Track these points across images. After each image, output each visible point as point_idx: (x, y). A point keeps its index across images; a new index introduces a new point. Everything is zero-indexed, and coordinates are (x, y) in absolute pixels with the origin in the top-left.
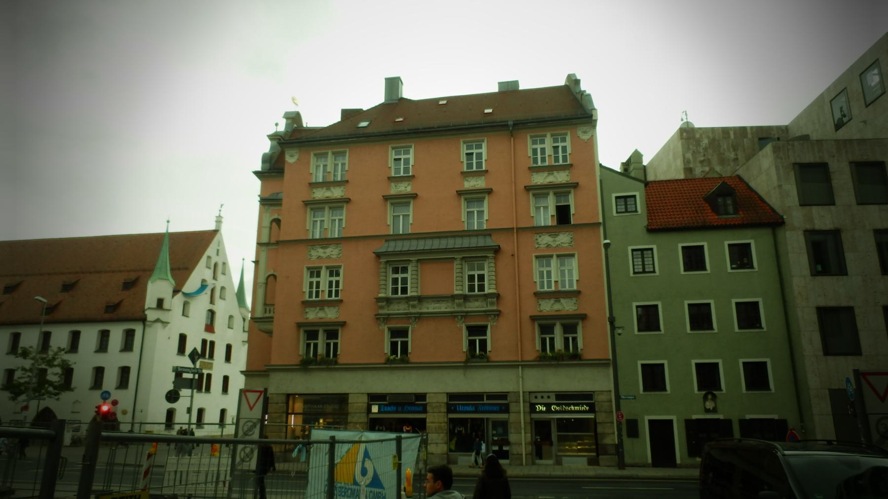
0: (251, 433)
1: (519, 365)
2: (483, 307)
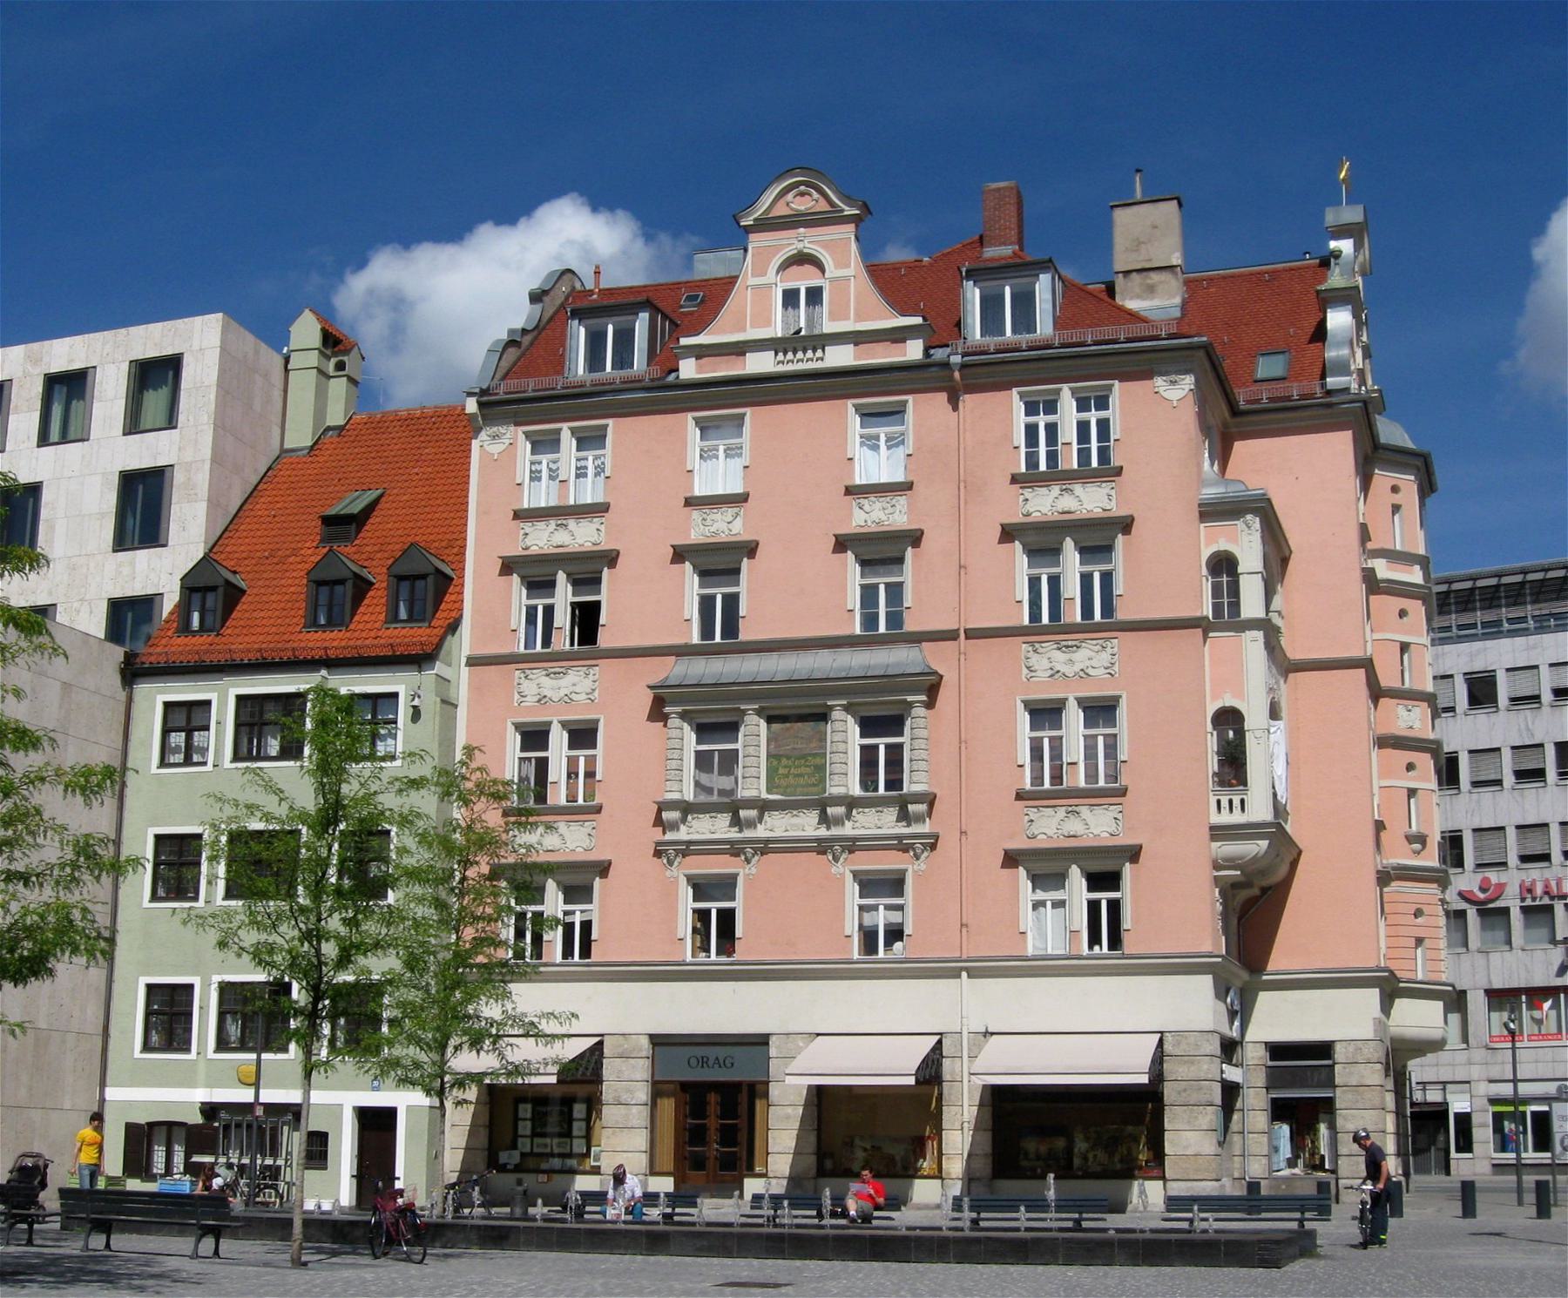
1: (962, 969)
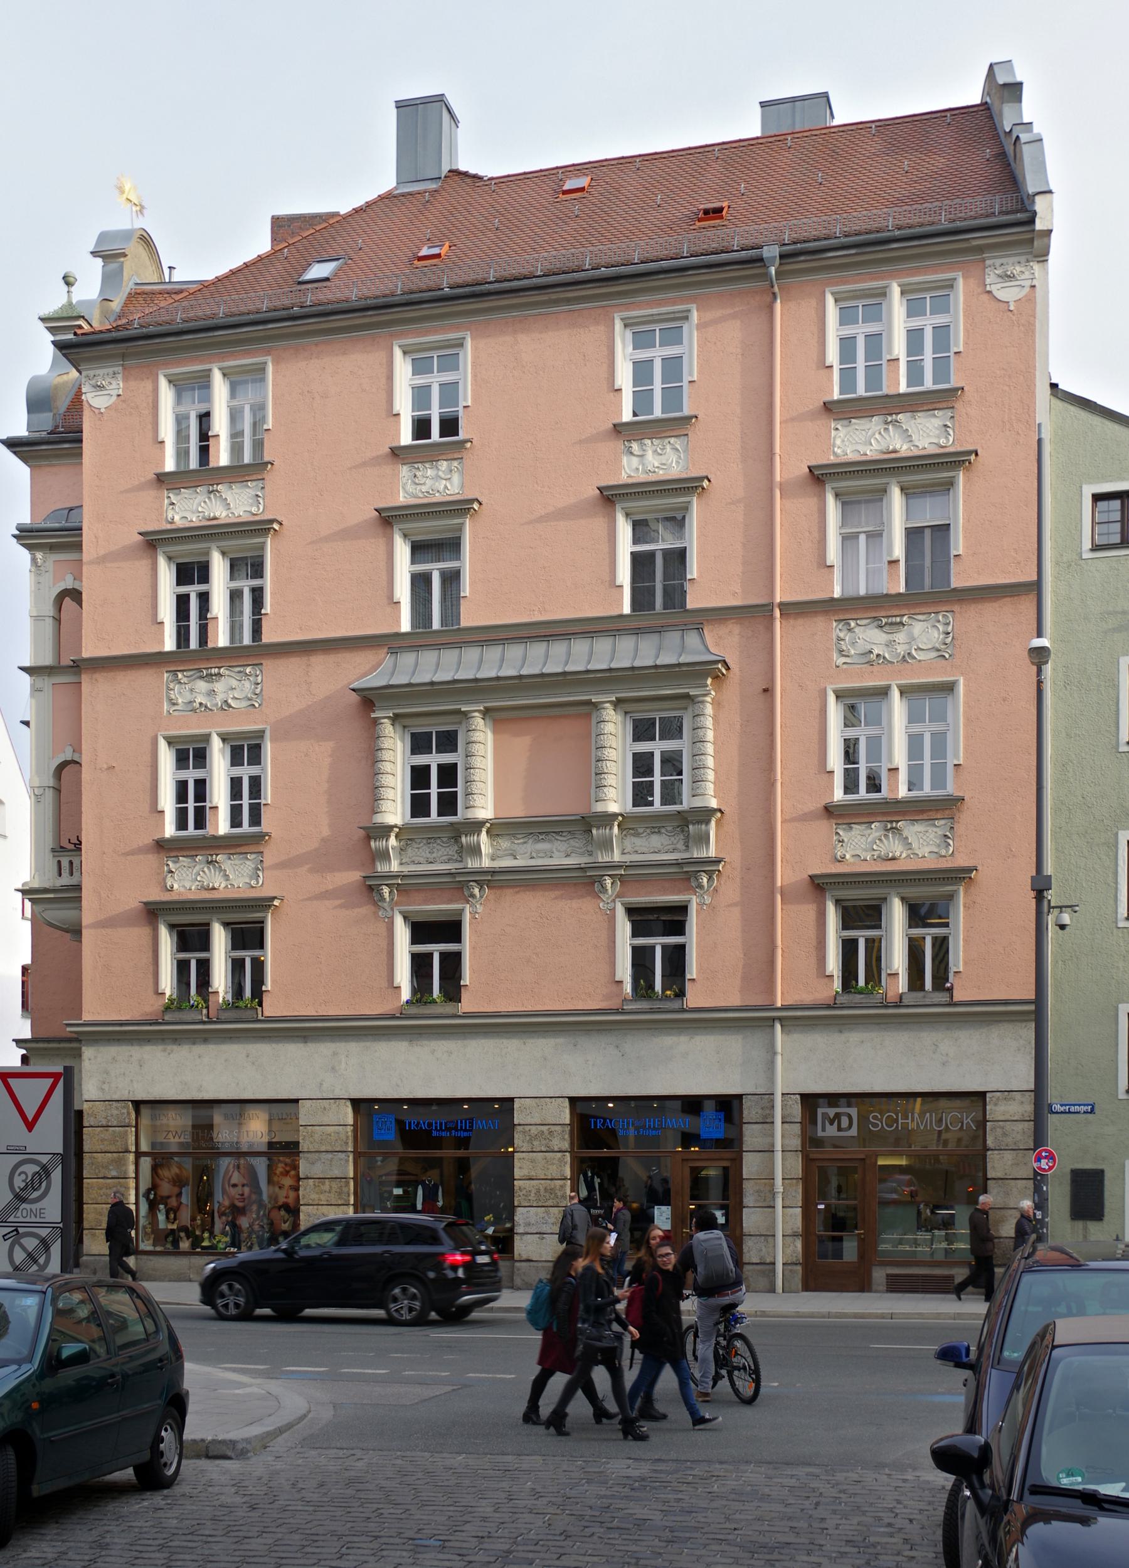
0: (36, 1194)
1: (773, 1019)
2: (674, 850)
